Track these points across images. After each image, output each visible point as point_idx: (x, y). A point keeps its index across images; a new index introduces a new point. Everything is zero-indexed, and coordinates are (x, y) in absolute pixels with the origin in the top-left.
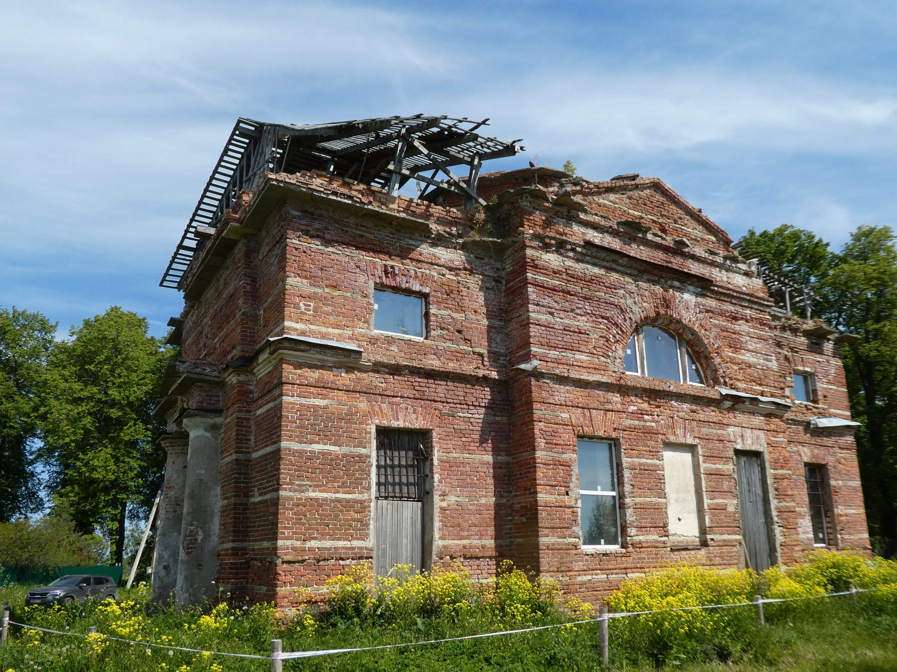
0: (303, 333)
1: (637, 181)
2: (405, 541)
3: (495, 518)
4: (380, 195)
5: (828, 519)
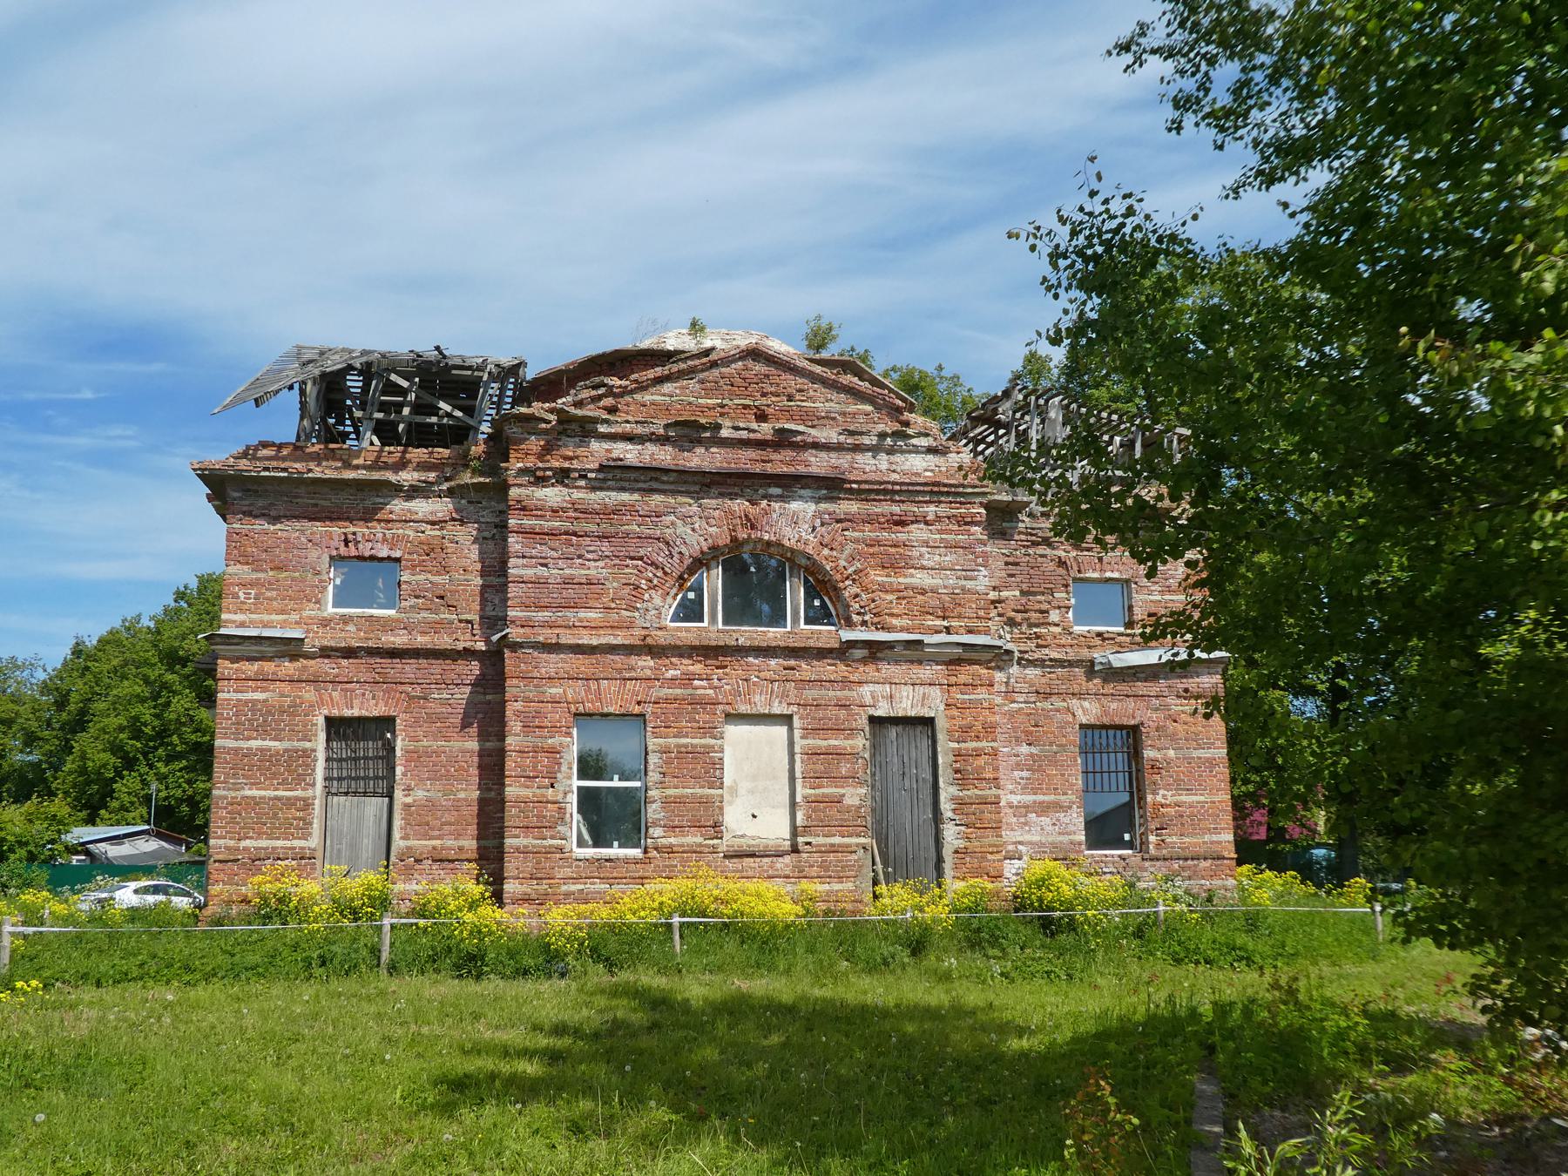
0: (242, 625)
1: (713, 356)
3: (479, 815)
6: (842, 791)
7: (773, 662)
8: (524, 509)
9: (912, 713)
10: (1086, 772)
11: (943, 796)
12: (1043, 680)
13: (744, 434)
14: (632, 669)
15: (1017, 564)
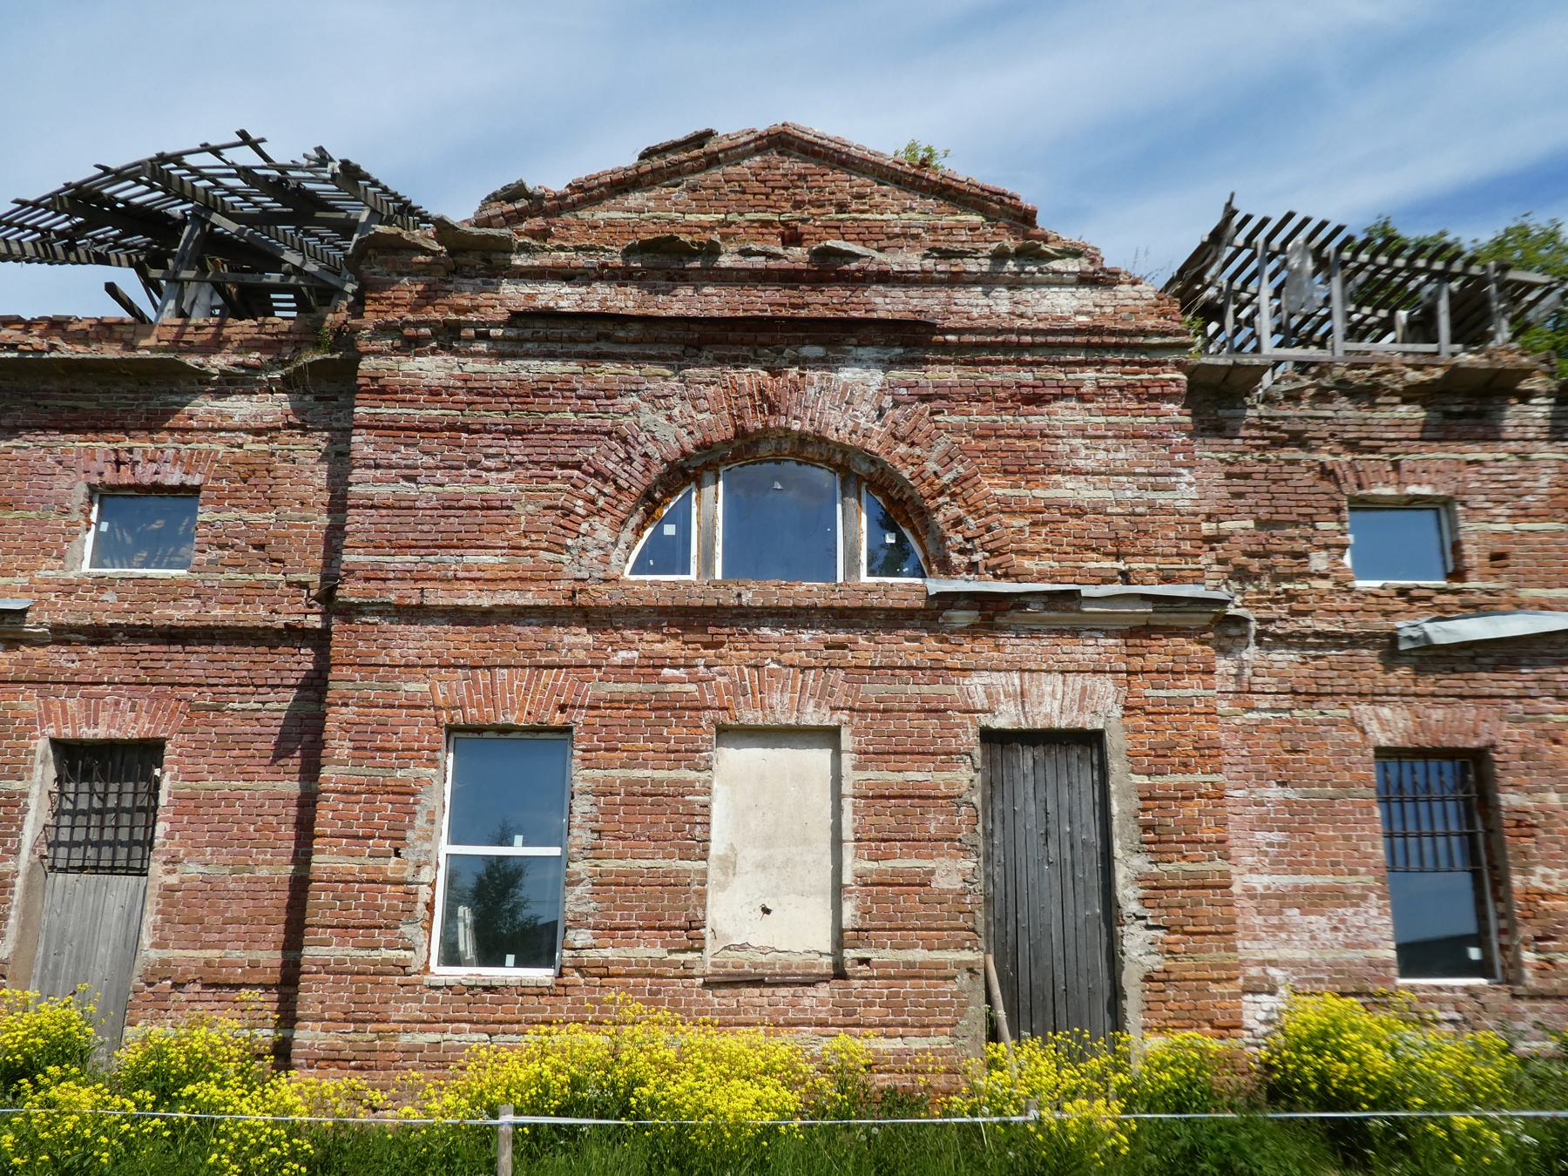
2: (102, 950)
4: (122, 329)
5: (1501, 907)
6: (929, 864)
7: (806, 636)
8: (383, 390)
9: (1061, 723)
10: (1390, 835)
11: (1121, 874)
12: (1305, 671)
13: (759, 262)
14: (553, 649)
15: (1247, 476)
